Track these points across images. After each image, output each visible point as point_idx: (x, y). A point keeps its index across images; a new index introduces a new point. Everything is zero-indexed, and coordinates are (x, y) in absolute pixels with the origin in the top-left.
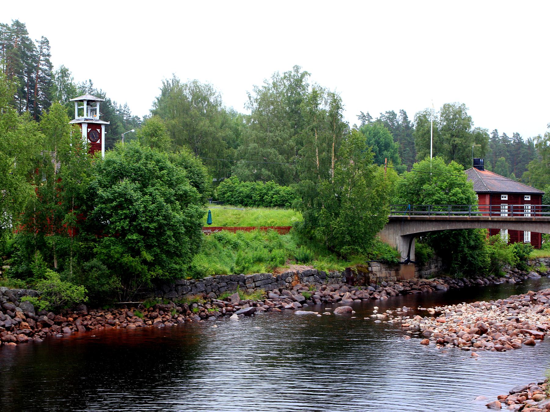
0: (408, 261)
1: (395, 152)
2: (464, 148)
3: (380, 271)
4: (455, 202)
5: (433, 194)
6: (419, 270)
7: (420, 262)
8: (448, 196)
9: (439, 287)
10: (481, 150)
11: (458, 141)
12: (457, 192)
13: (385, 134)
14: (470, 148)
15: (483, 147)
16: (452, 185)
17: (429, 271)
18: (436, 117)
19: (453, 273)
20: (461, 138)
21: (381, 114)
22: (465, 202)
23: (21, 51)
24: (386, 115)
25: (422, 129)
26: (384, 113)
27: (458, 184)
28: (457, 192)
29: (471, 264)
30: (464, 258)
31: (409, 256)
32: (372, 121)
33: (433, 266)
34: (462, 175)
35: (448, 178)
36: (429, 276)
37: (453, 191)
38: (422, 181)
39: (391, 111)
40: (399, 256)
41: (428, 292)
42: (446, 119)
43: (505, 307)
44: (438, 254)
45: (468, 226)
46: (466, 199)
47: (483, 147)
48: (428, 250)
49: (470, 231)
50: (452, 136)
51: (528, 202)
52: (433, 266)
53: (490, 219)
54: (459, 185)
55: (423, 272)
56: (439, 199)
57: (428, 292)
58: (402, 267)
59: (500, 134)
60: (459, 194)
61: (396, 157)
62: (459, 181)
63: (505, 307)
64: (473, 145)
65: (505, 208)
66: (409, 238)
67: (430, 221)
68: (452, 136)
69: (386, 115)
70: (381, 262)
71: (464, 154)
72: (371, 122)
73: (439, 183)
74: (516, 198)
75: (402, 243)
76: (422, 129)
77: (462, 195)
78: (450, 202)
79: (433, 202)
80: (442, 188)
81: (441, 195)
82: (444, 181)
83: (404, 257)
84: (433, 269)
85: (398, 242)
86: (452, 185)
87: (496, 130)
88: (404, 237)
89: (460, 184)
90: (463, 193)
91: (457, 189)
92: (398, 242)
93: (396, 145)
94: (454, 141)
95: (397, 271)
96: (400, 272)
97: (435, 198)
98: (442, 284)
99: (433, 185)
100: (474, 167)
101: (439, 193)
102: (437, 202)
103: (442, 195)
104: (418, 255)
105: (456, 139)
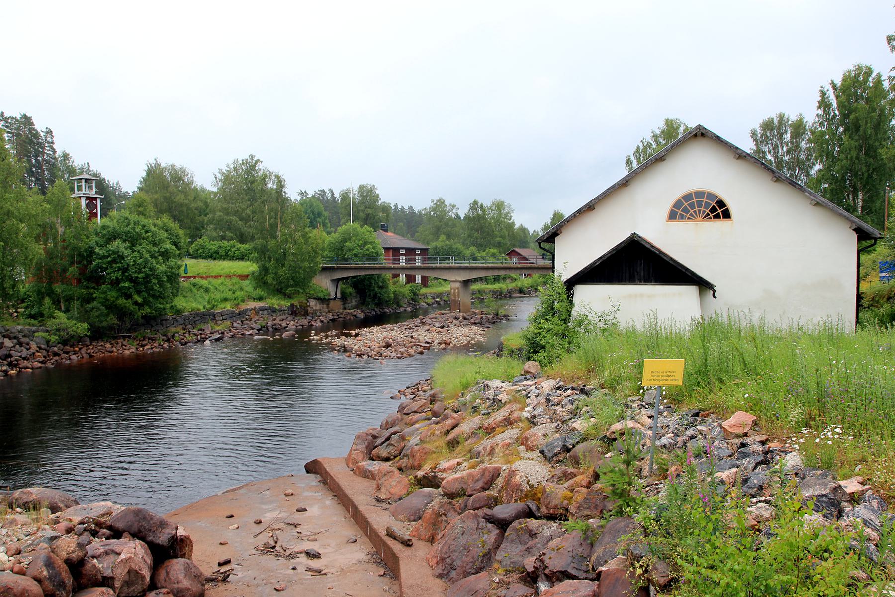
0: (336, 298)
4: (368, 255)
7: (344, 298)
11: (370, 211)
15: (387, 216)
16: (366, 243)
29: (380, 299)
37: (366, 247)
38: (345, 241)
45: (378, 272)
47: (387, 216)
48: (350, 290)
54: (371, 243)
58: (332, 302)
59: (400, 207)
62: (371, 240)
63: (404, 328)
64: (381, 214)
65: (403, 259)
66: (336, 281)
74: (410, 251)
78: (364, 255)
81: (358, 250)
83: (333, 296)
84: (354, 303)
86: (366, 243)
88: (332, 280)
90: (374, 248)
95: (328, 305)
96: (330, 306)
102: (356, 255)
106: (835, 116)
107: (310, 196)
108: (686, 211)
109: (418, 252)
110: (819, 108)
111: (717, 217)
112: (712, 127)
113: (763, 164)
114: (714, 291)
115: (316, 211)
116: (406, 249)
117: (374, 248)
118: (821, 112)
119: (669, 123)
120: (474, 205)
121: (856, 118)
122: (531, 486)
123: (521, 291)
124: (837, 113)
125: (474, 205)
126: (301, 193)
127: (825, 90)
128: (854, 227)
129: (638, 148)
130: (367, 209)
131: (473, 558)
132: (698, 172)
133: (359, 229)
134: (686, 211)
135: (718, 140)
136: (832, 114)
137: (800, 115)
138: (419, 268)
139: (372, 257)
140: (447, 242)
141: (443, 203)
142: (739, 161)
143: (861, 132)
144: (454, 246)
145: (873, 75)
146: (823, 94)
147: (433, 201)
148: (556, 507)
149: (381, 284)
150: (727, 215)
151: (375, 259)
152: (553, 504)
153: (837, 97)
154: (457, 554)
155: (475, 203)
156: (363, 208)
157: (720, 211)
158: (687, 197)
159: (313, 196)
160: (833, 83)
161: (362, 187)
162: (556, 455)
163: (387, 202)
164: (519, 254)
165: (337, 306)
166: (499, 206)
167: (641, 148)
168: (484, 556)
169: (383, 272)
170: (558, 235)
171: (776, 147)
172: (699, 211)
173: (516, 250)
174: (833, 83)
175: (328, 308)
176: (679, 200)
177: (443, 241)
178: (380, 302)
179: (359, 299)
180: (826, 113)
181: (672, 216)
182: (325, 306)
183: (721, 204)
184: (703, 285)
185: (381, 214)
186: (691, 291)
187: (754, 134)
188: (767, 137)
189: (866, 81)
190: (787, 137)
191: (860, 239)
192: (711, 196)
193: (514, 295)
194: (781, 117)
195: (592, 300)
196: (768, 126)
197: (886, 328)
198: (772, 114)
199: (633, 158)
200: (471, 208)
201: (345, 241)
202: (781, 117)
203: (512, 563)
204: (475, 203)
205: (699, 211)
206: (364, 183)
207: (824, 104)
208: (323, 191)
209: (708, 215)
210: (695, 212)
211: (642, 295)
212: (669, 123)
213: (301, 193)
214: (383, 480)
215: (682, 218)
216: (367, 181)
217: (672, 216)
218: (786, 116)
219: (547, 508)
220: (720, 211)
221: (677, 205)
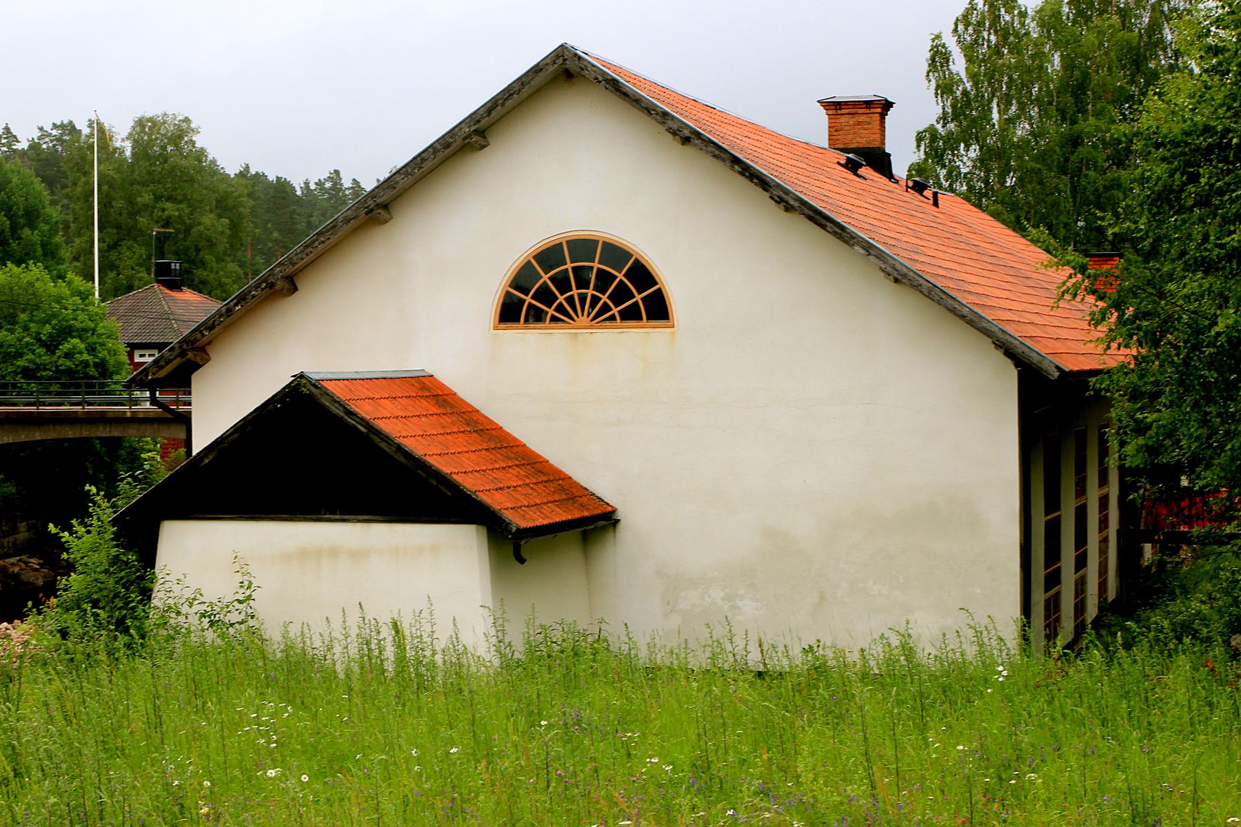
1: (53, 231)
2: (188, 230)
4: (69, 371)
5: (19, 355)
8: (54, 358)
10: (228, 232)
12: (74, 347)
13: (24, 184)
14: (201, 228)
15: (235, 227)
16: (66, 332)
17: (11, 539)
20: (181, 202)
21: (41, 129)
22: (92, 371)
24: (54, 132)
25: (83, 180)
26: (48, 128)
27: (78, 330)
28: (74, 347)
32: (19, 146)
33: (22, 526)
34: (91, 308)
35: (54, 316)
36: (11, 551)
37: (66, 347)
39: (66, 122)
45: (103, 432)
46: (96, 365)
47: (235, 227)
50: (158, 198)
52: (22, 526)
53: (129, 415)
54: (82, 333)
56: (31, 366)
59: (347, 183)
60: (80, 353)
61: (58, 246)
62: (82, 321)
64: (208, 219)
69: (54, 132)
71: (188, 243)
72: (15, 151)
73: (34, 327)
76: (83, 180)
77: (85, 357)
79: (17, 374)
80: (39, 340)
82: (45, 322)
86: (66, 332)
87: (337, 172)
89: (86, 330)
91: (76, 341)
93: (54, 213)
94: (163, 210)
97: (21, 363)
98: (36, 570)
100: (158, 282)
101: (33, 352)
102: (27, 373)
103: (40, 356)
105: (168, 205)
107: (23, 145)
108: (545, 295)
111: (631, 315)
112: (600, 46)
115: (19, 202)
130: (282, 186)
132: (576, 185)
135: (617, 88)
139: (82, 380)
142: (685, 147)
150: (658, 309)
156: (146, 198)
157: (638, 297)
158: (548, 256)
159: (34, 146)
161: (145, 128)
169: (131, 434)
170: (196, 367)
172: (583, 299)
176: (527, 267)
181: (509, 313)
183: (642, 275)
185: (208, 219)
192: (615, 253)
199: (951, 42)
206: (151, 110)
208: (70, 129)
209: (606, 308)
210: (570, 300)
211: (334, 552)
215: (536, 316)
216: (163, 104)
217: (509, 313)
220: (638, 297)
221: (521, 280)
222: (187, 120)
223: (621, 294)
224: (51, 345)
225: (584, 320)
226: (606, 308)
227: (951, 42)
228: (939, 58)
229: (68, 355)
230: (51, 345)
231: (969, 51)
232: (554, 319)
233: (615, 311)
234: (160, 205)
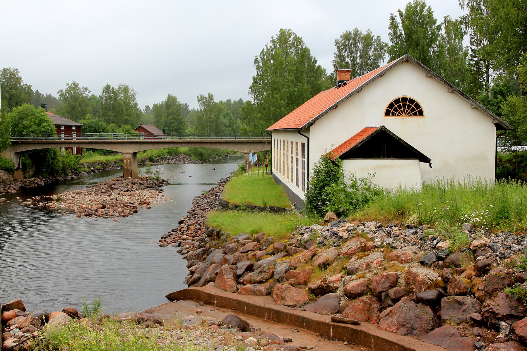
0: (19, 168)
3: (4, 175)
5: (30, 127)
6: (24, 174)
7: (24, 168)
9: (39, 183)
11: (14, 92)
18: (96, 91)
19: (42, 174)
23: (11, 79)
29: (52, 168)
30: (49, 165)
31: (19, 165)
33: (31, 170)
38: (22, 119)
40: (14, 165)
41: (34, 186)
42: (5, 78)
43: (100, 192)
44: (33, 163)
48: (28, 161)
49: (47, 150)
51: (74, 131)
52: (31, 170)
54: (46, 122)
55: (26, 175)
57: (34, 186)
58: (15, 172)
63: (100, 192)
65: (63, 134)
66: (19, 154)
67: (34, 143)
68: (10, 89)
70: (5, 170)
74: (68, 128)
75: (15, 157)
78: (41, 132)
81: (34, 128)
82: (36, 119)
83: (16, 166)
84: (31, 173)
85: (12, 157)
88: (16, 153)
90: (49, 126)
92: (12, 157)
95: (13, 174)
96: (14, 175)
97: (31, 129)
99: (30, 121)
102: (33, 132)
104: (24, 165)
105: (13, 91)
106: (401, 34)
109: (74, 128)
110: (389, 28)
111: (415, 114)
113: (445, 81)
114: (430, 164)
116: (65, 126)
117: (49, 126)
118: (392, 32)
119: (282, 32)
120: (107, 89)
121: (417, 37)
122: (432, 280)
123: (151, 160)
124: (403, 33)
125: (107, 89)
126: (201, 99)
127: (394, 16)
128: (496, 122)
129: (263, 50)
131: (426, 321)
133: (34, 109)
134: (396, 110)
136: (399, 33)
137: (369, 30)
138: (74, 143)
140: (93, 120)
141: (77, 85)
142: (429, 79)
143: (420, 47)
144: (100, 124)
145: (426, 8)
146: (393, 19)
147: (68, 84)
148: (464, 288)
149: (53, 156)
150: (421, 113)
151: (49, 135)
152: (462, 286)
153: (403, 22)
154: (412, 321)
155: (108, 87)
160: (400, 11)
162: (434, 262)
163: (28, 84)
164: (145, 130)
165: (19, 174)
166: (126, 89)
167: (266, 50)
168: (432, 319)
169: (57, 147)
171: (352, 53)
173: (143, 126)
174: (400, 11)
175: (13, 177)
176: (392, 103)
177: (89, 119)
178: (52, 171)
179: (34, 169)
180: (395, 32)
181: (387, 113)
182: (11, 176)
183: (418, 106)
184: (424, 159)
186: (414, 163)
187: (337, 43)
188: (346, 45)
189: (421, 11)
190: (360, 46)
191: (497, 129)
193: (146, 163)
194: (356, 31)
195: (355, 170)
196: (346, 37)
197: (517, 183)
198: (350, 29)
199: (259, 58)
200: (104, 91)
201: (22, 119)
202: (356, 31)
203: (458, 319)
204: (108, 87)
205: (404, 110)
207: (393, 26)
209: (409, 113)
211: (385, 166)
212: (282, 32)
213: (201, 99)
214: (285, 293)
215: (393, 114)
218: (359, 31)
219: (459, 289)
221: (391, 106)
222: (16, 69)
223: (413, 110)
224: (39, 125)
225: (404, 115)
226: (409, 113)
227: (259, 58)
228: (256, 61)
229: (43, 127)
230: (39, 125)
231: (263, 60)
232: (398, 115)
233: (411, 113)
234: (11, 90)
